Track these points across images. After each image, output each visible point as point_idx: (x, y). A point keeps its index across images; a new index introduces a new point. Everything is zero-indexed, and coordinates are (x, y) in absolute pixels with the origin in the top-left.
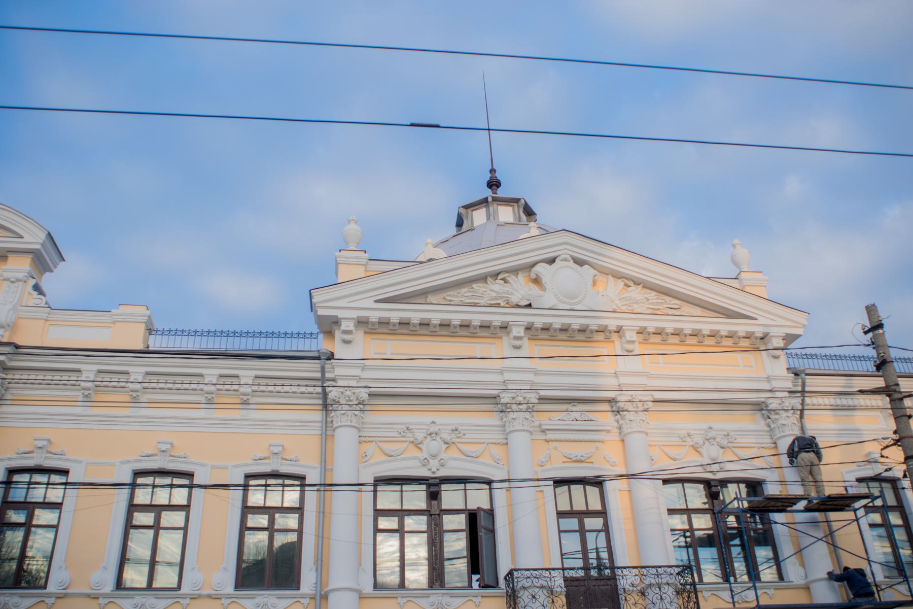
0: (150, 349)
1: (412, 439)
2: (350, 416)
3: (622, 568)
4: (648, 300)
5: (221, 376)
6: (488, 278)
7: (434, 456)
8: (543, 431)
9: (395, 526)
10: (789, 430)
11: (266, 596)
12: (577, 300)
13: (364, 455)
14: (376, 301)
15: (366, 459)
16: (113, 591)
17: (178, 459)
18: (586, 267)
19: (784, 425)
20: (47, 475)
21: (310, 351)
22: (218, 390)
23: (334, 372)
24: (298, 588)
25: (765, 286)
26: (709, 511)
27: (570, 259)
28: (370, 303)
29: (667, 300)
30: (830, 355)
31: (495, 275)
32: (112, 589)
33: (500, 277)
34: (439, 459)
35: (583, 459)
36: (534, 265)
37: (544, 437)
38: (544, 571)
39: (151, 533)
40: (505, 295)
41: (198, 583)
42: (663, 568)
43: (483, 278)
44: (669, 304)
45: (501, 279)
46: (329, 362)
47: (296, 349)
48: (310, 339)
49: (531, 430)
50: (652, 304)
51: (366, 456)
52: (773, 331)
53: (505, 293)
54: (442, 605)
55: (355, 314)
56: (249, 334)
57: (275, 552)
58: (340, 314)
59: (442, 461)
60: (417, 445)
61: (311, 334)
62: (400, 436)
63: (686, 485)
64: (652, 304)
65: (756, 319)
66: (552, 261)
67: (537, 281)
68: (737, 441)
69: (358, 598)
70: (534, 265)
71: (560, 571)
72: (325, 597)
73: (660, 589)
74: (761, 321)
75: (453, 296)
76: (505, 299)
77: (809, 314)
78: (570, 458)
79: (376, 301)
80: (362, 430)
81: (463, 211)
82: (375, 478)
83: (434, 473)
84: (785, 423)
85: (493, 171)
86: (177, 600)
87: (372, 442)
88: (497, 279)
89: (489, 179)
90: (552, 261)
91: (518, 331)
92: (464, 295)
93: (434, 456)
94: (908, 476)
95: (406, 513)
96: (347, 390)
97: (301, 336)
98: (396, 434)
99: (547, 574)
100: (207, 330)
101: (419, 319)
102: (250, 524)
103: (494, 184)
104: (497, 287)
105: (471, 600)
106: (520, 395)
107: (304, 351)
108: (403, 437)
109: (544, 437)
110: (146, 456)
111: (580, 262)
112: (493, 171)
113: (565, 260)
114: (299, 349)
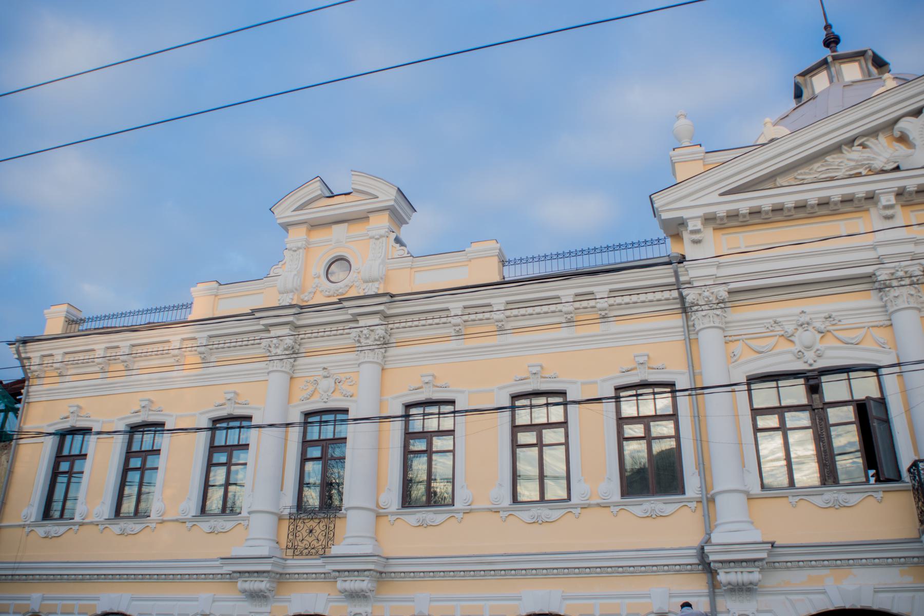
0: (506, 279)
5: (576, 295)
7: (809, 348)
11: (652, 502)
13: (732, 355)
14: (721, 195)
15: (735, 358)
17: (549, 379)
23: (688, 275)
28: (715, 198)
30: (589, 249)
31: (851, 142)
32: (509, 503)
33: (856, 143)
34: (815, 350)
36: (896, 121)
39: (535, 450)
43: (837, 148)
46: (681, 265)
54: (840, 503)
55: (700, 212)
58: (685, 214)
60: (789, 338)
61: (659, 240)
67: (903, 139)
70: (896, 121)
72: (711, 500)
79: (721, 195)
82: (614, 387)
83: (811, 365)
85: (828, 27)
86: (870, 494)
88: (853, 146)
89: (824, 37)
91: (888, 199)
93: (809, 348)
95: (786, 410)
97: (610, 249)
98: (764, 330)
100: (606, 246)
101: (770, 205)
103: (831, 41)
104: (855, 154)
105: (872, 496)
106: (900, 270)
108: (772, 331)
112: (828, 27)
114: (648, 257)
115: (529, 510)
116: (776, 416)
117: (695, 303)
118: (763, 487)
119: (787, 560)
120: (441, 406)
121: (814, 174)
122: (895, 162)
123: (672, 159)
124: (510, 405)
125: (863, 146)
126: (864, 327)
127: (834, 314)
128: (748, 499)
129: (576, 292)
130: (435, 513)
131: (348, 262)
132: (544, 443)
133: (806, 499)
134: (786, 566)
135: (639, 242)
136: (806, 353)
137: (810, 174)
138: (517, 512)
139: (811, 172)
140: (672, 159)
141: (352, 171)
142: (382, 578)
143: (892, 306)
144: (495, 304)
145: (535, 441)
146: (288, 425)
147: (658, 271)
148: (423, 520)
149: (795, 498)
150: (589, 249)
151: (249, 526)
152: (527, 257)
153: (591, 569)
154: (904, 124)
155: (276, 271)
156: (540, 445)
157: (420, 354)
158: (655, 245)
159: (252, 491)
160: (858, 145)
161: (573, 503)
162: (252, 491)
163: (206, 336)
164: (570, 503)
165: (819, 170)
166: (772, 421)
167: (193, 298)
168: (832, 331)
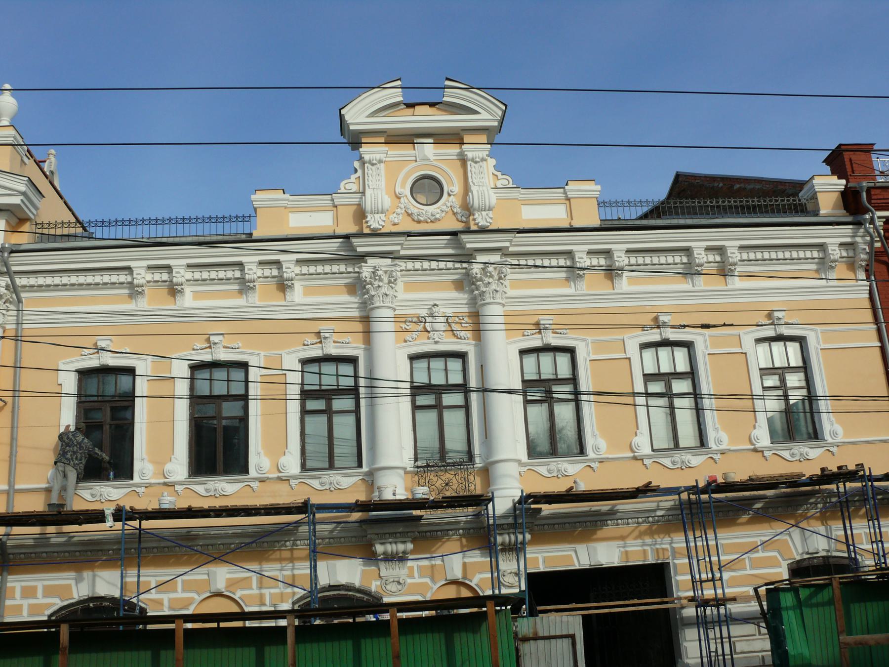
2: (381, 297)
5: (148, 268)
9: (433, 403)
10: (500, 298)
11: (216, 482)
16: (185, 479)
17: (232, 350)
19: (387, 295)
20: (209, 370)
21: (631, 220)
22: (296, 275)
24: (132, 479)
26: (569, 381)
30: (96, 221)
32: (185, 477)
41: (835, 438)
47: (115, 238)
48: (169, 225)
49: (503, 302)
54: (562, 473)
56: (118, 223)
63: (675, 348)
69: (52, 491)
80: (506, 305)
82: (408, 355)
84: (388, 293)
100: (155, 219)
102: (418, 403)
106: (379, 269)
107: (612, 220)
110: (88, 354)
114: (117, 238)
115: (206, 484)
116: (663, 383)
117: (368, 281)
118: (653, 450)
120: (540, 354)
129: (259, 259)
130: (230, 482)
131: (814, 176)
132: (444, 404)
133: (533, 469)
134: (638, 521)
135: (190, 218)
138: (661, 459)
141: (447, 79)
142: (297, 546)
143: (481, 301)
144: (576, 251)
145: (324, 408)
146: (446, 370)
147: (122, 253)
150: (96, 221)
151: (645, 468)
153: (37, 554)
155: (348, 186)
156: (439, 407)
158: (132, 225)
159: (486, 438)
161: (252, 477)
162: (486, 438)
163: (185, 264)
164: (248, 476)
166: (320, 405)
167: (816, 192)
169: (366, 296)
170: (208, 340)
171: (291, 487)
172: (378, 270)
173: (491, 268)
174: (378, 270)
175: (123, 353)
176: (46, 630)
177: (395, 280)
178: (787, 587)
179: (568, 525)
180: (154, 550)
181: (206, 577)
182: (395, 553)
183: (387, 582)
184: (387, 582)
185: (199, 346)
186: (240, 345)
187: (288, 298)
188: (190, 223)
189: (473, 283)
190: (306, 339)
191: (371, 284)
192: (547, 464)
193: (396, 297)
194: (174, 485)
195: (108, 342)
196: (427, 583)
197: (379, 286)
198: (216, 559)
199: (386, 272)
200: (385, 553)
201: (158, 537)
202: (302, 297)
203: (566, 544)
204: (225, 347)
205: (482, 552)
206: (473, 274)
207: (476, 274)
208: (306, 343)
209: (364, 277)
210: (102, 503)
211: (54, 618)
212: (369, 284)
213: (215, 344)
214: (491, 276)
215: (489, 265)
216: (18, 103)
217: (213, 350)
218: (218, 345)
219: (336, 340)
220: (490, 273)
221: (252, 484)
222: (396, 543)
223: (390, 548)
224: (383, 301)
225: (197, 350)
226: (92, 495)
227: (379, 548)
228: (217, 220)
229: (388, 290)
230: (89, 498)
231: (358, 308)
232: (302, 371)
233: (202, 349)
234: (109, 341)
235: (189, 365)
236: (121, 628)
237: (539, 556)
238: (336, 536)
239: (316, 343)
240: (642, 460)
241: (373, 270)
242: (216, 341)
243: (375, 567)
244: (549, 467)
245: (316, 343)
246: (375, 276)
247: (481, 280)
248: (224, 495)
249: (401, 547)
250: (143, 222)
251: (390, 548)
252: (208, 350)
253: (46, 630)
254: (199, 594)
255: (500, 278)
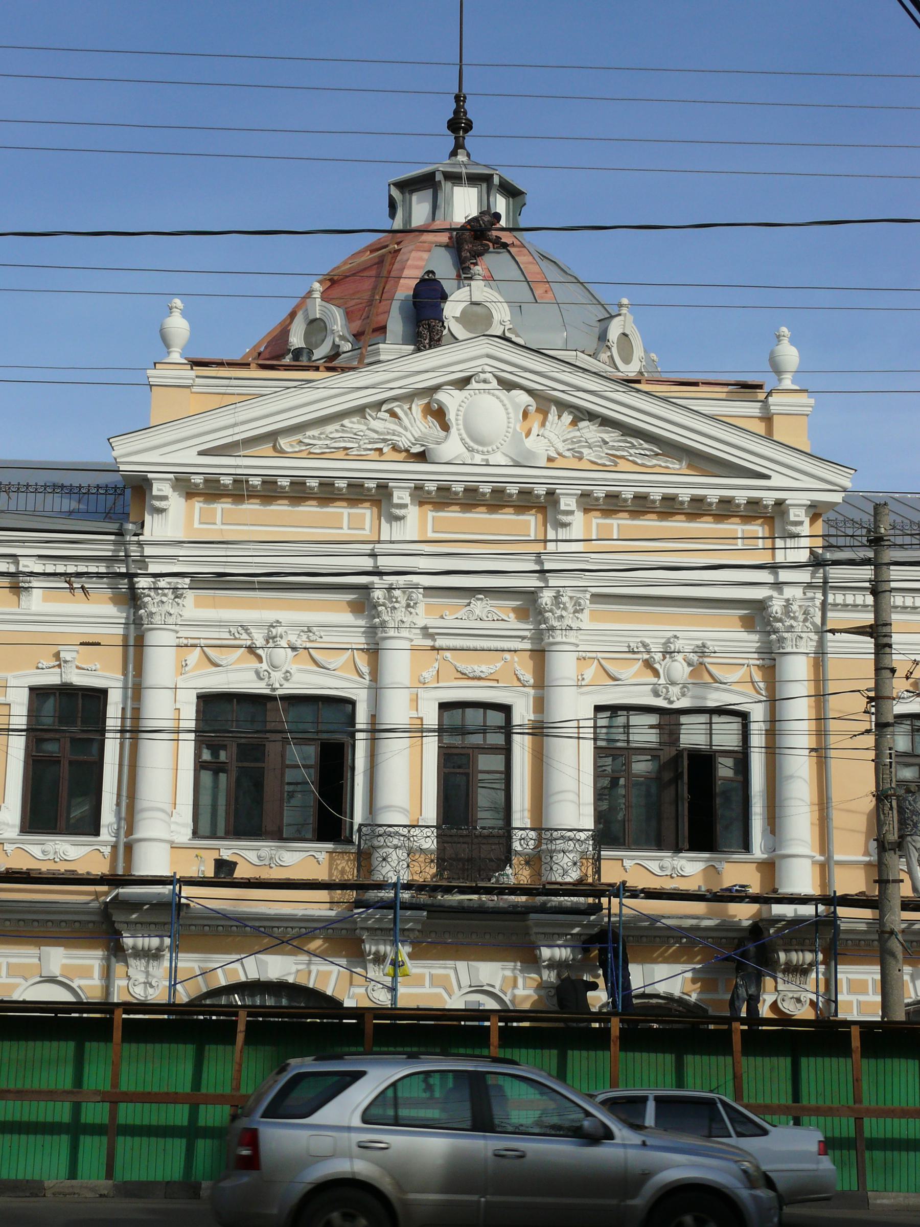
1: (249, 643)
3: (551, 829)
4: (606, 443)
6: (368, 410)
8: (432, 636)
11: (57, 842)
12: (485, 449)
13: (184, 664)
14: (201, 453)
18: (515, 392)
25: (807, 415)
27: (489, 376)
29: (636, 444)
33: (384, 408)
34: (284, 670)
35: (483, 676)
37: (429, 643)
38: (401, 828)
40: (388, 437)
42: (559, 832)
43: (360, 411)
44: (637, 449)
45: (385, 411)
50: (613, 448)
51: (186, 665)
52: (790, 498)
53: (388, 433)
57: (490, 233)
59: (288, 674)
62: (232, 637)
64: (613, 448)
65: (768, 477)
66: (463, 383)
67: (439, 414)
68: (325, 639)
70: (436, 388)
71: (432, 829)
73: (551, 858)
74: (777, 481)
75: (314, 437)
76: (390, 442)
77: (856, 471)
78: (463, 674)
79: (201, 453)
81: (395, 193)
87: (195, 646)
88: (380, 411)
90: (463, 383)
92: (331, 436)
94: (286, 794)
96: (159, 581)
98: (227, 636)
99: (405, 831)
104: (380, 423)
109: (429, 643)
111: (508, 385)
113: (485, 381)
119: (709, 936)
121: (325, 439)
122: (423, 445)
123: (150, 379)
124: (657, 723)
125: (393, 414)
126: (744, 665)
127: (709, 643)
128: (172, 847)
135: (19, 485)
136: (273, 673)
137: (320, 439)
138: (646, 862)
139: (322, 436)
140: (150, 379)
148: (56, 853)
149: (227, 851)
152: (36, 484)
154: (441, 396)
157: (87, 617)
160: (385, 411)
164: (99, 839)
165: (331, 436)
168: (706, 664)
169: (377, 620)
170: (57, 655)
171: (318, 861)
172: (562, 596)
173: (397, 593)
174: (792, 604)
175: (83, 669)
176: (166, 1017)
177: (416, 604)
178: (557, 1028)
179: (140, 925)
180: (76, 924)
181: (36, 961)
182: (141, 948)
183: (136, 983)
184: (136, 983)
185: (45, 664)
186: (98, 666)
187: (22, 603)
188: (36, 491)
189: (769, 623)
190: (42, 661)
191: (384, 605)
192: (660, 859)
193: (181, 616)
194: (3, 844)
195: (74, 655)
196: (441, 994)
197: (562, 617)
198: (283, 942)
199: (571, 598)
200: (134, 948)
201: (219, 913)
202: (424, 616)
203: (32, 947)
204: (78, 667)
205: (350, 959)
206: (374, 598)
207: (378, 599)
208: (40, 665)
209: (774, 612)
210: (56, 862)
211: (605, 1010)
212: (381, 605)
213: (66, 662)
214: (565, 609)
215: (161, 579)
216: (799, 352)
217: (63, 670)
218: (69, 664)
219: (79, 665)
220: (564, 604)
221: (317, 855)
222: (802, 951)
223: (142, 942)
224: (796, 645)
225: (43, 669)
226: (43, 852)
227: (546, 953)
228: (18, 489)
229: (405, 616)
230: (39, 855)
231: (364, 632)
232: (912, 735)
233: (50, 668)
234: (75, 653)
235: (197, 694)
236: (214, 1018)
237: (426, 971)
238: (136, 920)
239: (54, 667)
240: (622, 860)
241: (785, 604)
242: (68, 659)
243: (361, 968)
244: (662, 863)
245: (54, 667)
246: (558, 603)
247: (780, 620)
248: (66, 860)
249: (155, 942)
250: (45, 489)
251: (142, 942)
252: (57, 670)
253: (166, 1017)
254: (26, 979)
255: (576, 611)
